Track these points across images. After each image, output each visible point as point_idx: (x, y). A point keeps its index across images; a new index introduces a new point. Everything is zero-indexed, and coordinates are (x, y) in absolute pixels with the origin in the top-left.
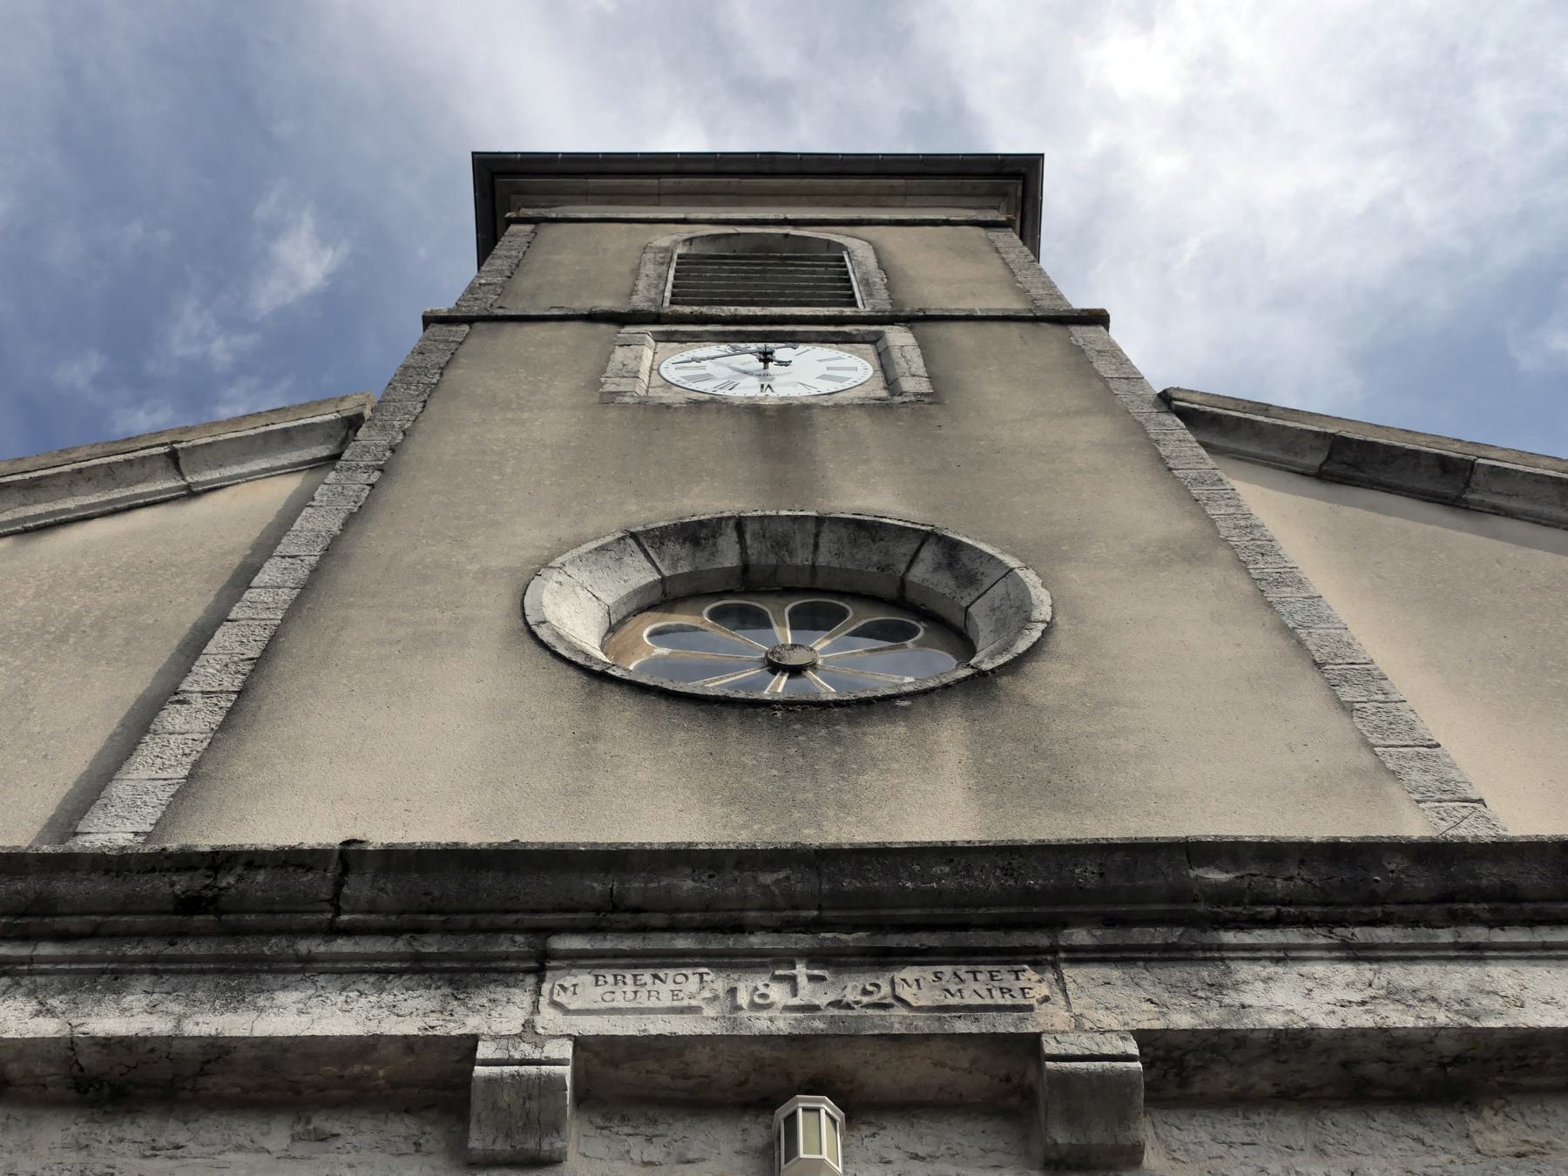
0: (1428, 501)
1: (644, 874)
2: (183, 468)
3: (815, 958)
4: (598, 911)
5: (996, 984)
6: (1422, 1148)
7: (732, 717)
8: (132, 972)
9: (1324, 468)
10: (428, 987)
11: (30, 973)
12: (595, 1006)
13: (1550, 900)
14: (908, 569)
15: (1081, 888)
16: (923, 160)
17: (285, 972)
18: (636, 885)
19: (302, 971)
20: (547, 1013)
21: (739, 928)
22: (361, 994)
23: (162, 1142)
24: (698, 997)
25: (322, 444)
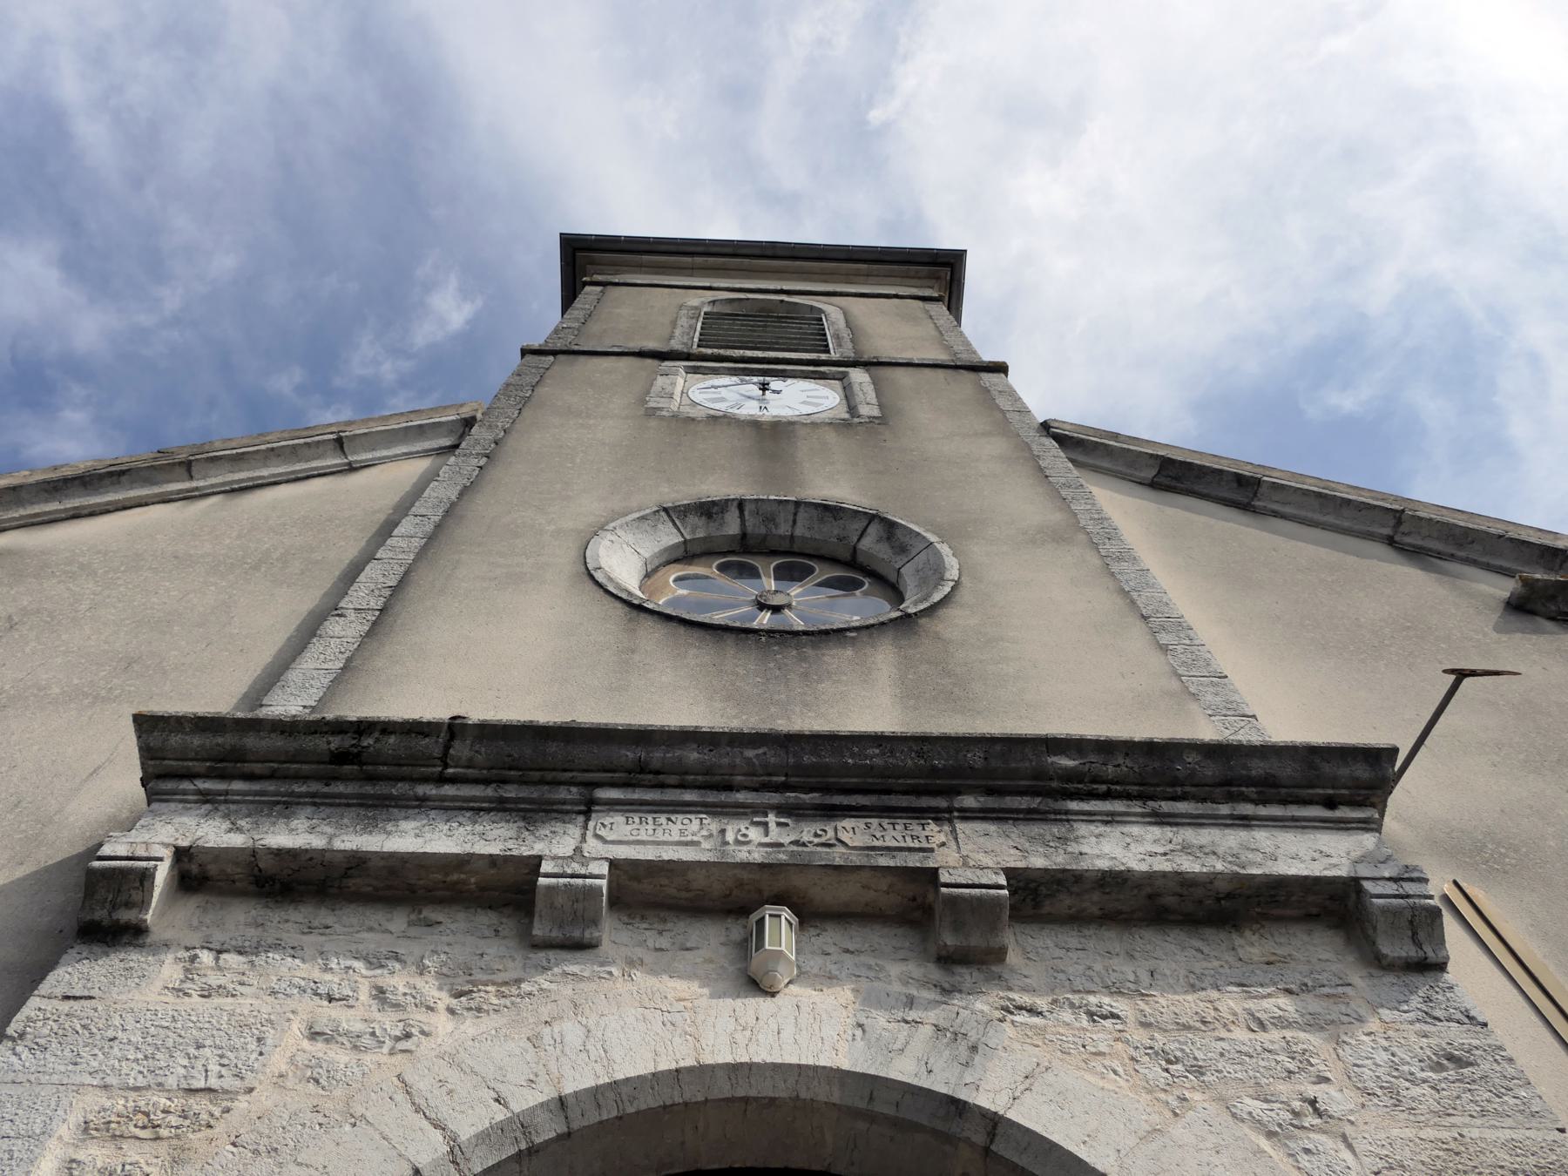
0: (1227, 505)
1: (663, 747)
5: (908, 832)
6: (1199, 955)
8: (298, 804)
10: (508, 821)
11: (226, 802)
14: (859, 540)
17: (408, 807)
18: (657, 755)
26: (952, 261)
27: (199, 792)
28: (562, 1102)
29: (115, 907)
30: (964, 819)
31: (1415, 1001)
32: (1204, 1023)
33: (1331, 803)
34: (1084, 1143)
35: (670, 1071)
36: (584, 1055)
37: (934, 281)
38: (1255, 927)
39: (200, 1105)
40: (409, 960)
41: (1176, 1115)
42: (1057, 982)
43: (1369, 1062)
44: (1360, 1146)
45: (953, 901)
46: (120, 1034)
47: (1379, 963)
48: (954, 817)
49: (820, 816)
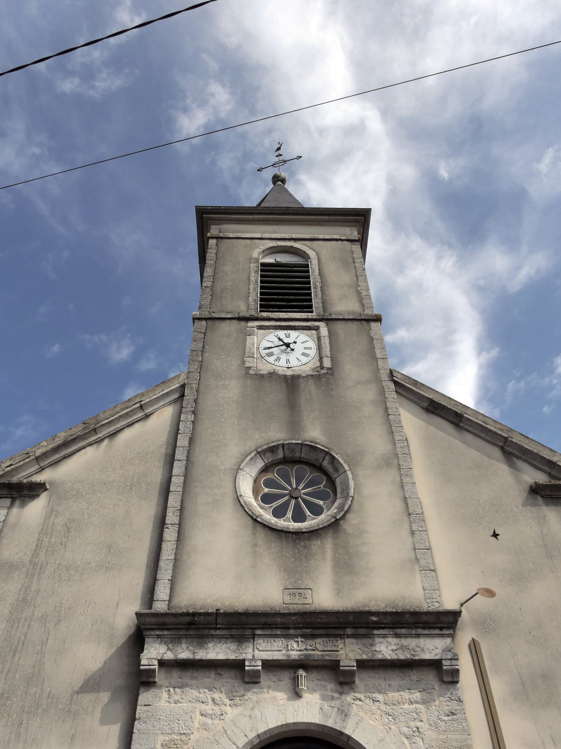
0: (451, 423)
2: (143, 408)
3: (303, 636)
5: (333, 644)
6: (401, 679)
7: (283, 535)
8: (182, 638)
9: (428, 408)
10: (234, 642)
11: (164, 638)
12: (264, 649)
13: (434, 624)
14: (322, 461)
16: (334, 210)
17: (209, 638)
19: (211, 637)
20: (256, 652)
21: (288, 628)
22: (223, 644)
23: (194, 676)
25: (176, 393)
26: (365, 214)
27: (156, 635)
28: (258, 735)
29: (148, 678)
30: (347, 637)
31: (449, 695)
32: (399, 703)
33: (441, 629)
34: (367, 743)
35: (280, 725)
36: (262, 721)
37: (356, 223)
38: (416, 668)
39: (183, 737)
40: (217, 688)
41: (388, 733)
42: (368, 690)
43: (433, 715)
44: (425, 741)
45: (344, 671)
46: (161, 717)
47: (443, 682)
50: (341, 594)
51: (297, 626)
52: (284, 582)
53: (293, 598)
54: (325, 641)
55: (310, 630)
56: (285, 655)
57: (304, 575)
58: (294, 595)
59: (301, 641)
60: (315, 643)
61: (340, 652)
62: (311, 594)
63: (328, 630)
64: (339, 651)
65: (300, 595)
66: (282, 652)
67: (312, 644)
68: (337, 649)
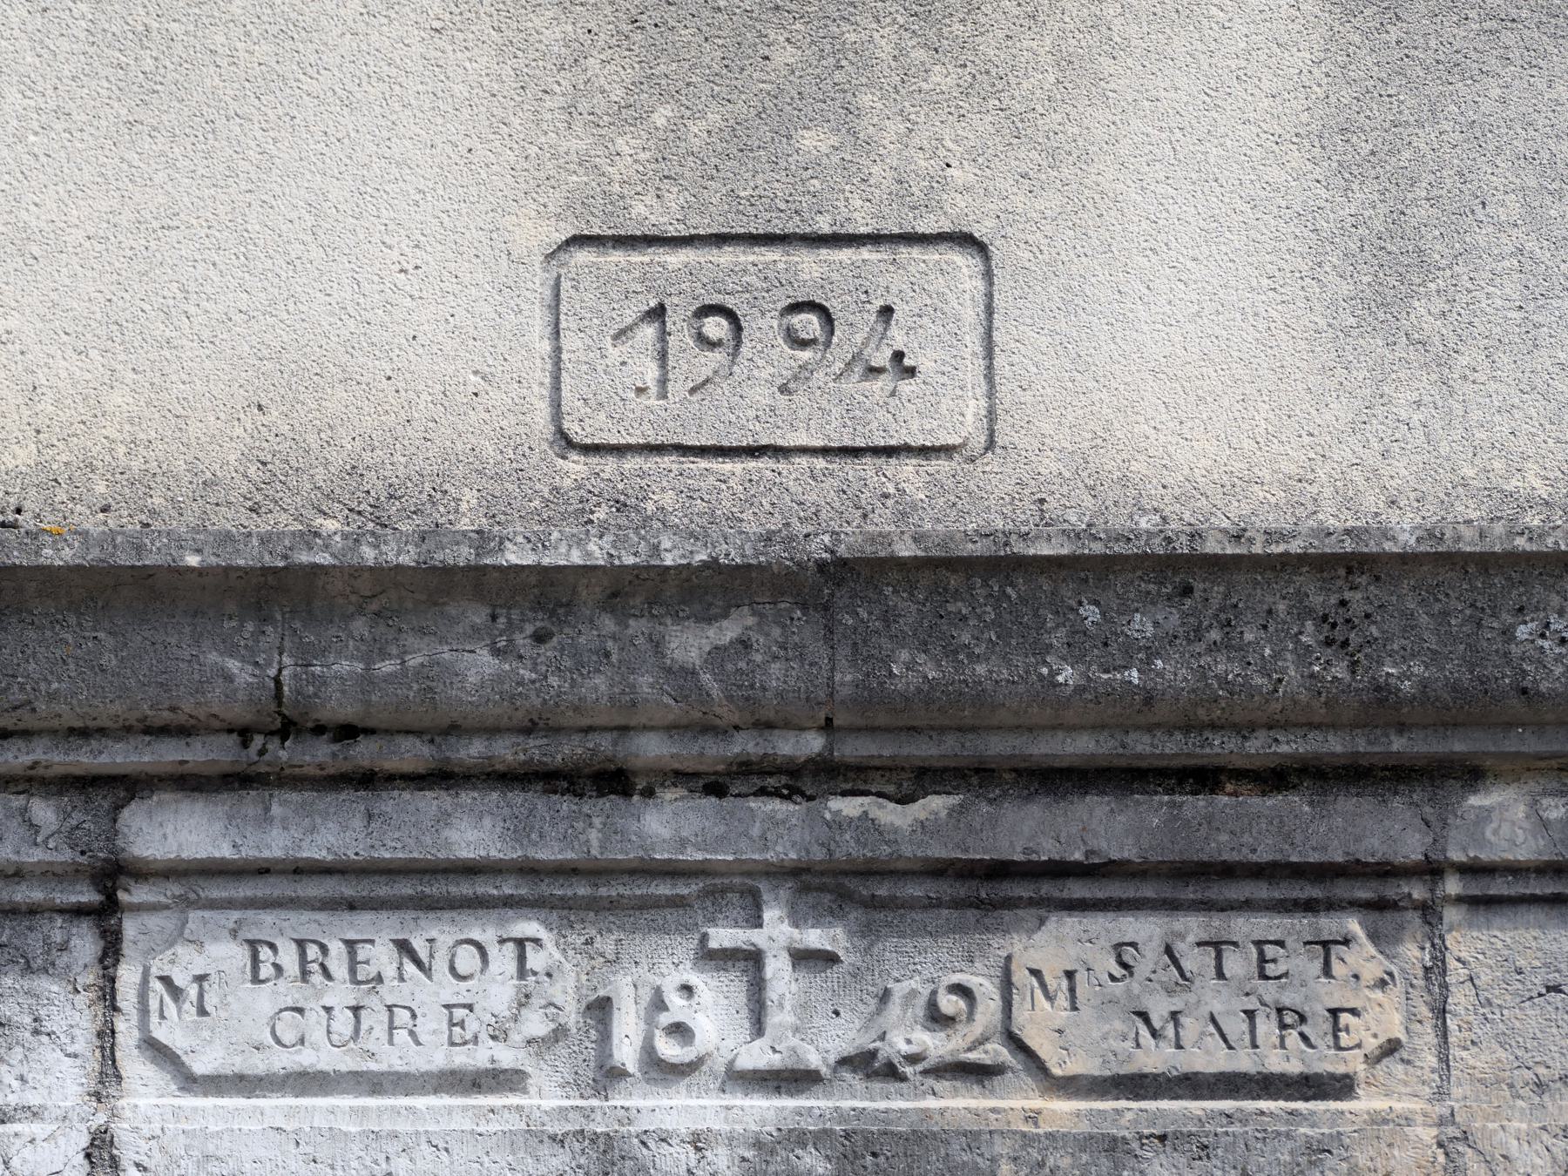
1: (360, 626)
4: (244, 734)
5: (1269, 990)
12: (257, 1064)
15: (1524, 691)
18: (344, 666)
24: (515, 1037)
30: (1478, 903)
48: (1447, 899)
49: (957, 904)
50: (1423, 314)
51: (745, 745)
52: (577, 143)
53: (692, 363)
54: (1149, 960)
55: (936, 804)
56: (558, 1140)
57: (885, 49)
58: (715, 327)
59: (803, 958)
60: (1007, 985)
61: (1365, 1103)
62: (971, 314)
63: (1195, 805)
64: (1341, 1086)
65: (809, 324)
66: (513, 1100)
67: (962, 990)
68: (1326, 1063)
